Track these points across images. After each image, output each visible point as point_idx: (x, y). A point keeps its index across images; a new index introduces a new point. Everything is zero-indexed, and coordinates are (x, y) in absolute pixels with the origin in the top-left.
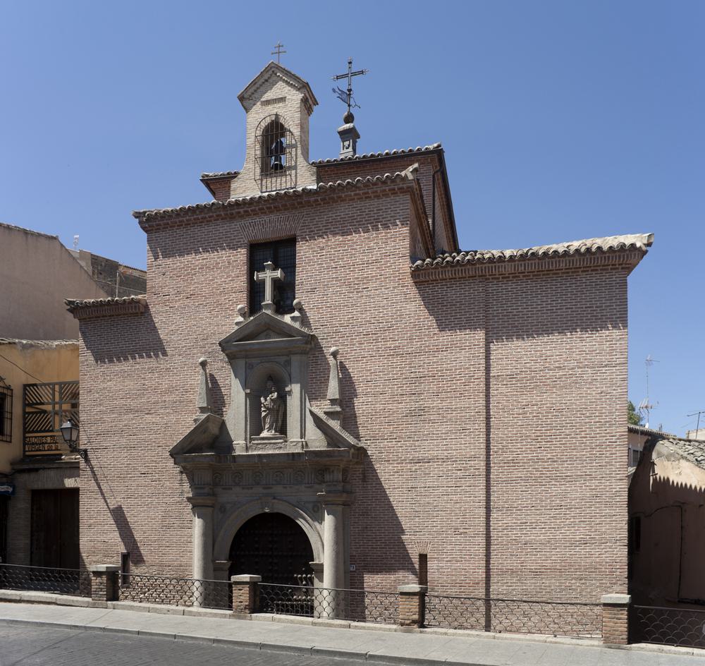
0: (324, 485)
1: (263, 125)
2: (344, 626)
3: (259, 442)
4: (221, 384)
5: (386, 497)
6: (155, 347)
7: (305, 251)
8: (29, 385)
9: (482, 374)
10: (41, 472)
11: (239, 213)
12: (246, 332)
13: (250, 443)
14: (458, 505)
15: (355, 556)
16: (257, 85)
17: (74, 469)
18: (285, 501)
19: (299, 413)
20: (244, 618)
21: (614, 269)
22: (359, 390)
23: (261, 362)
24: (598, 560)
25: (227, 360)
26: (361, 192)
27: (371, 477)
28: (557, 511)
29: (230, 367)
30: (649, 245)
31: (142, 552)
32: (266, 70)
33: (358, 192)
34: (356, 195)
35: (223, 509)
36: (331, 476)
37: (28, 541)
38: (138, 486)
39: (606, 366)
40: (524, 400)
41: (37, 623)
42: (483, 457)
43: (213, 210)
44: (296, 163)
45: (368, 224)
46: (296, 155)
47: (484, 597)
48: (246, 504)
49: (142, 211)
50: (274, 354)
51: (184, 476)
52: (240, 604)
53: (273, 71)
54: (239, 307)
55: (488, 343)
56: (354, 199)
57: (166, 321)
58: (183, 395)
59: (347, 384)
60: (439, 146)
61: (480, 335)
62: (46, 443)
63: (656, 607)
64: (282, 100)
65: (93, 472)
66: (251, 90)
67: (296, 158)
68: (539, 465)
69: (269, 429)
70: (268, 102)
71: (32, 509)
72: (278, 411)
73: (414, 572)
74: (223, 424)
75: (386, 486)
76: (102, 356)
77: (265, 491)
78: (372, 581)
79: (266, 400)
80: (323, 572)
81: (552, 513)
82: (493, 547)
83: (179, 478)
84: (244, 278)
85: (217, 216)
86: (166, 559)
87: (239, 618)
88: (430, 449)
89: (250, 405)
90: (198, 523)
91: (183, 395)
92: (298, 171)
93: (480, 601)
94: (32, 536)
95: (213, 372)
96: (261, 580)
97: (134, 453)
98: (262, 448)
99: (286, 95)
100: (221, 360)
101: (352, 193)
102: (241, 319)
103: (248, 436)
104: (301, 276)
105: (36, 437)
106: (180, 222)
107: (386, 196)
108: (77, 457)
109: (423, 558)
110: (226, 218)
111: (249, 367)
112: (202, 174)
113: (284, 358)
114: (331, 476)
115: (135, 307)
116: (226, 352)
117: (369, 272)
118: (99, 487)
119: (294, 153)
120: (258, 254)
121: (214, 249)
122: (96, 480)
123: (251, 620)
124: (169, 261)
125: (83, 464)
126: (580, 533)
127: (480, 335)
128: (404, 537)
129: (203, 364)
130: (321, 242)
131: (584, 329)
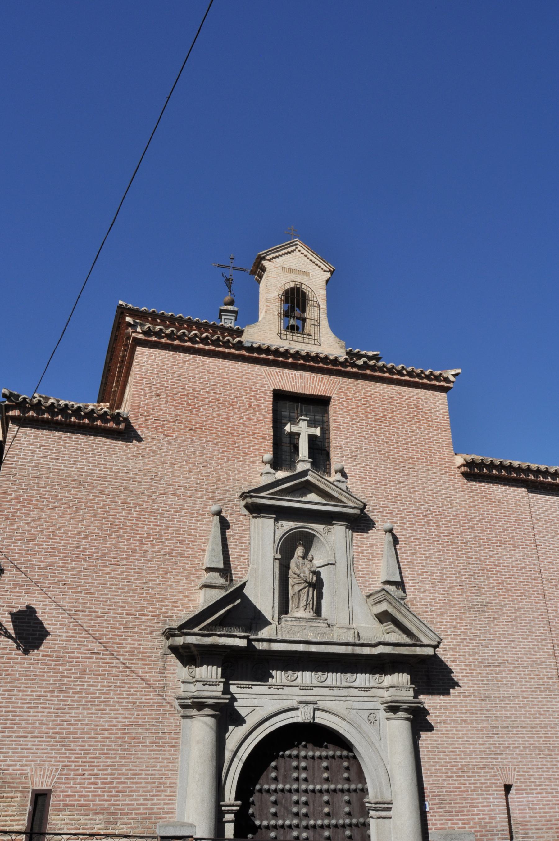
1: (287, 287)
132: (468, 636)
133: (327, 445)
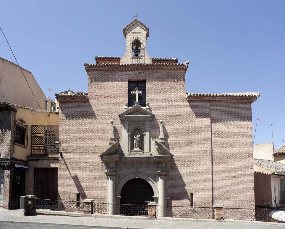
0: (159, 169)
1: (133, 40)
2: (195, 221)
3: (134, 152)
4: (118, 130)
5: (179, 173)
6: (91, 115)
7: (149, 85)
8: (34, 126)
9: (210, 132)
10: (40, 161)
11: (126, 69)
12: (130, 112)
13: (130, 152)
14: (203, 176)
15: (169, 194)
16: (130, 26)
17: (56, 160)
19: (149, 142)
20: (154, 219)
21: (248, 102)
22: (169, 136)
23: (134, 123)
24: (246, 194)
25: (120, 121)
26: (170, 68)
28: (233, 178)
30: (259, 96)
31: (86, 193)
32: (134, 22)
33: (168, 67)
34: (168, 68)
35: (119, 177)
36: (162, 166)
37: (33, 189)
38: (84, 167)
39: (246, 133)
40: (223, 142)
41: (75, 225)
42: (211, 160)
43: (116, 67)
44: (145, 55)
46: (145, 52)
47: (212, 207)
48: (128, 175)
49: (87, 63)
50: (138, 120)
51: (103, 164)
52: (151, 214)
53: (136, 22)
55: (211, 123)
56: (167, 70)
57: (95, 105)
60: (177, 59)
61: (209, 120)
62: (41, 149)
63: (263, 210)
64: (139, 32)
65: (64, 161)
66: (129, 27)
67: (145, 53)
68: (228, 163)
69: (137, 148)
70: (134, 33)
71: (35, 176)
72: (140, 141)
73: (189, 199)
74: (119, 145)
75: (179, 169)
76: (68, 117)
77: (136, 170)
78: (174, 203)
79: (136, 137)
80: (158, 200)
81: (232, 179)
82: (214, 190)
83: (101, 165)
84: (127, 92)
85: (117, 69)
86: (96, 196)
87: (151, 219)
88: (194, 157)
89: (130, 139)
90: (110, 183)
92: (146, 58)
93: (211, 208)
94: (34, 186)
95: (115, 126)
96: (36, 197)
97: (82, 154)
98: (135, 155)
99: (141, 31)
100: (118, 121)
101: (167, 68)
102: (126, 107)
103: (129, 150)
104: (148, 94)
105: (37, 147)
106: (102, 69)
107: (178, 70)
108: (59, 155)
109: (192, 194)
110: (120, 70)
111: (130, 125)
112: (96, 56)
113: (143, 122)
114: (162, 166)
115: (84, 99)
116: (121, 119)
118: (67, 167)
119: (144, 51)
120: (133, 84)
121: (115, 81)
122: (66, 165)
123: (157, 220)
124: (97, 83)
125: (60, 158)
126: (241, 185)
127: (209, 120)
128: (185, 187)
129: (112, 122)
130: (155, 83)
131: (240, 121)
132: (184, 153)
133: (139, 100)
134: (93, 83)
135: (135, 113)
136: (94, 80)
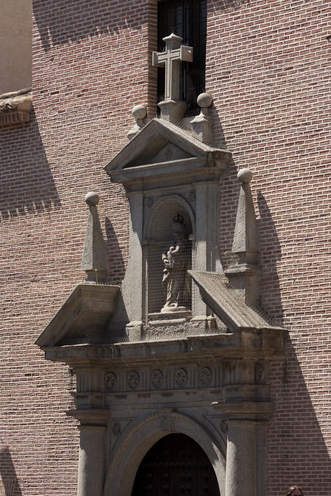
3: (157, 322)
12: (137, 151)
18: (188, 415)
23: (163, 196)
27: (293, 375)
29: (128, 204)
45: (96, 26)
54: (135, 108)
58: (74, 250)
59: (263, 233)
69: (172, 301)
91: (74, 250)
104: (211, 54)
111: (148, 203)
117: (296, 41)
129: (92, 203)
134: (51, 53)
135: (164, 151)
136: (54, 37)
